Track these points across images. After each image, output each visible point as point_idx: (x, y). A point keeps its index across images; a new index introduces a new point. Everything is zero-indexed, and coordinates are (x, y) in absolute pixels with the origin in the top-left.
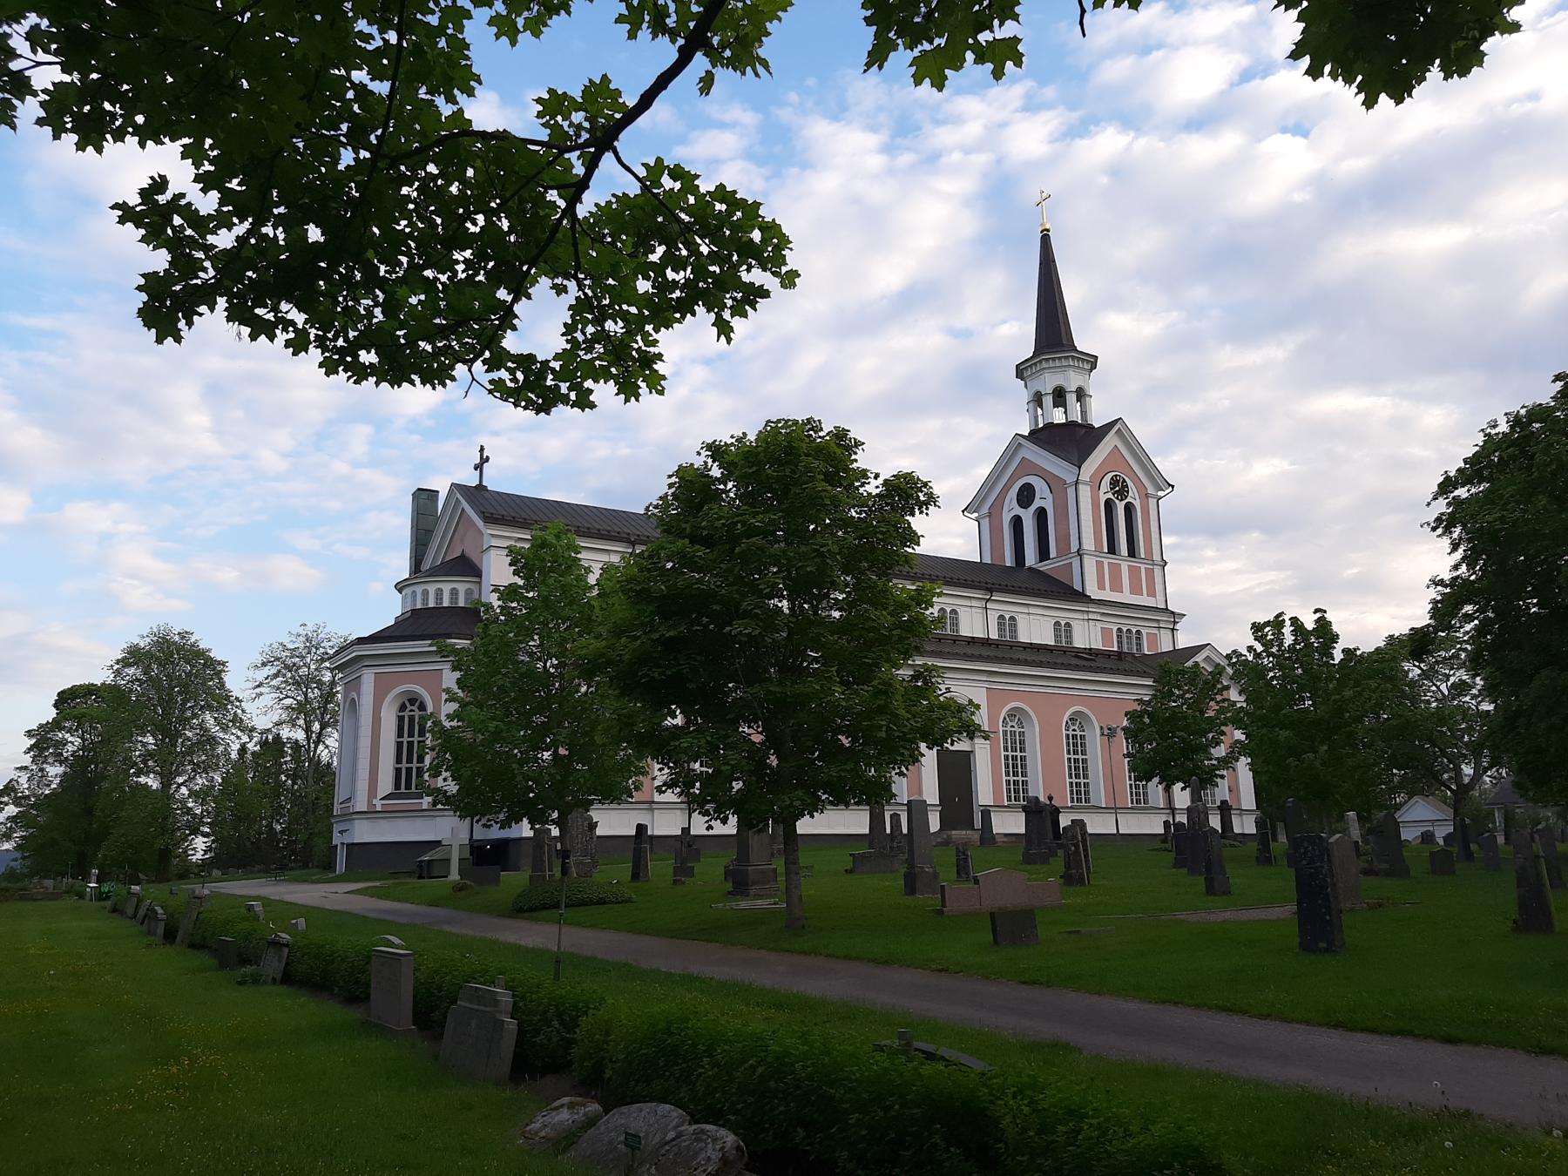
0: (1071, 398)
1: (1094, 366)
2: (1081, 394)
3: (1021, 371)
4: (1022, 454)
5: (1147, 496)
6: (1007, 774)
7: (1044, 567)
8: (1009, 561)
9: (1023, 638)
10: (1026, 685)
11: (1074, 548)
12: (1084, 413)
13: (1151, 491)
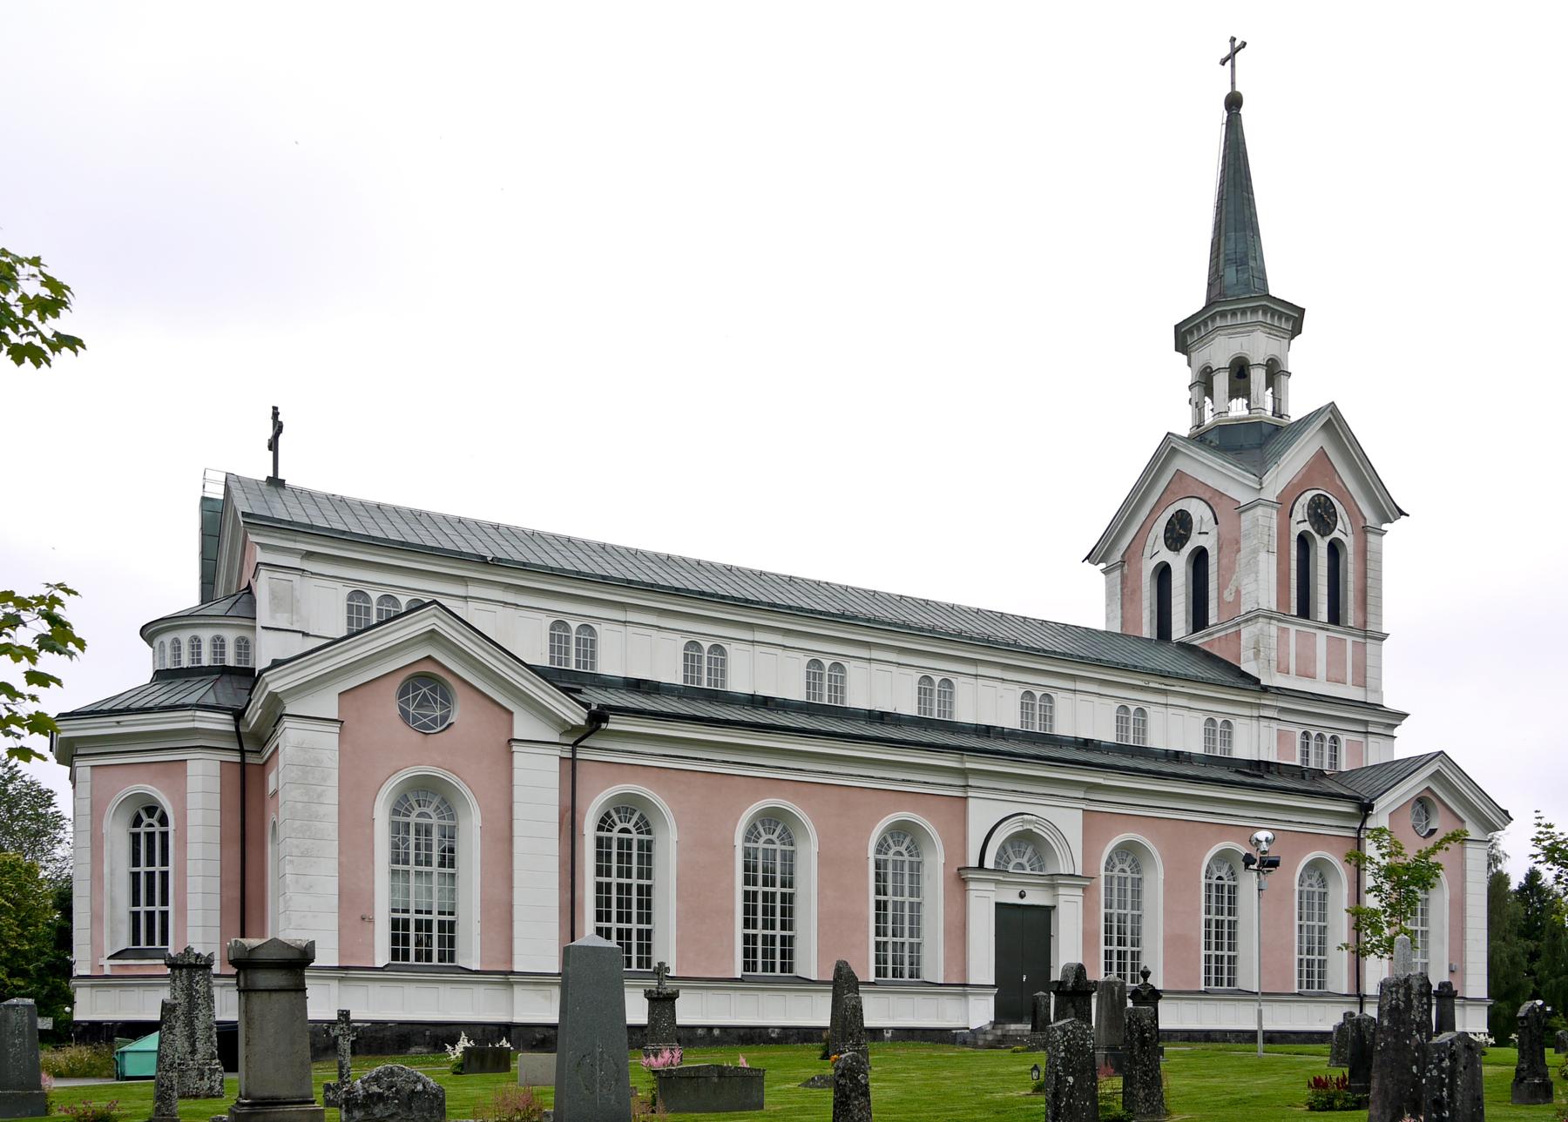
0: (1258, 377)
1: (1297, 330)
2: (1275, 372)
3: (1186, 336)
4: (1179, 463)
5: (1365, 529)
6: (1208, 947)
7: (1199, 640)
8: (1148, 630)
9: (1156, 741)
10: (890, 792)
11: (244, 585)
12: (1277, 400)
13: (1371, 520)
